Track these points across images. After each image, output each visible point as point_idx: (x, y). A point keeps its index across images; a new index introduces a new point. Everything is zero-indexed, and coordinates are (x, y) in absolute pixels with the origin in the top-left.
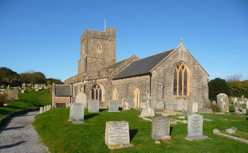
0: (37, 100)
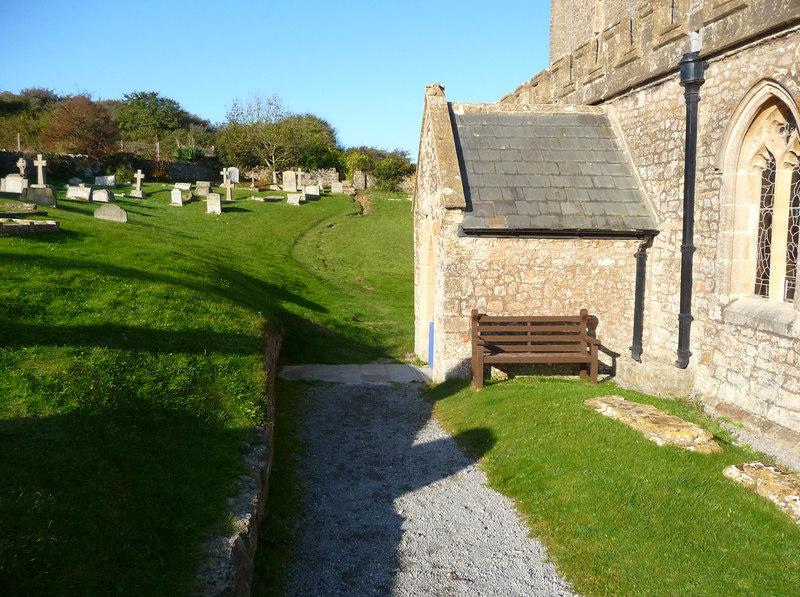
0: (288, 257)
